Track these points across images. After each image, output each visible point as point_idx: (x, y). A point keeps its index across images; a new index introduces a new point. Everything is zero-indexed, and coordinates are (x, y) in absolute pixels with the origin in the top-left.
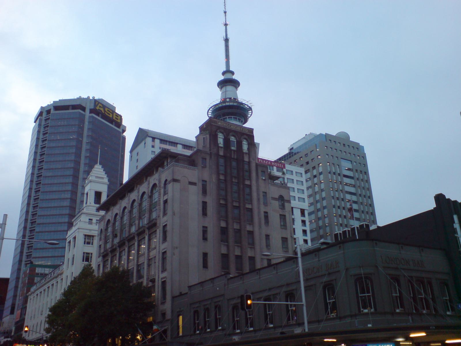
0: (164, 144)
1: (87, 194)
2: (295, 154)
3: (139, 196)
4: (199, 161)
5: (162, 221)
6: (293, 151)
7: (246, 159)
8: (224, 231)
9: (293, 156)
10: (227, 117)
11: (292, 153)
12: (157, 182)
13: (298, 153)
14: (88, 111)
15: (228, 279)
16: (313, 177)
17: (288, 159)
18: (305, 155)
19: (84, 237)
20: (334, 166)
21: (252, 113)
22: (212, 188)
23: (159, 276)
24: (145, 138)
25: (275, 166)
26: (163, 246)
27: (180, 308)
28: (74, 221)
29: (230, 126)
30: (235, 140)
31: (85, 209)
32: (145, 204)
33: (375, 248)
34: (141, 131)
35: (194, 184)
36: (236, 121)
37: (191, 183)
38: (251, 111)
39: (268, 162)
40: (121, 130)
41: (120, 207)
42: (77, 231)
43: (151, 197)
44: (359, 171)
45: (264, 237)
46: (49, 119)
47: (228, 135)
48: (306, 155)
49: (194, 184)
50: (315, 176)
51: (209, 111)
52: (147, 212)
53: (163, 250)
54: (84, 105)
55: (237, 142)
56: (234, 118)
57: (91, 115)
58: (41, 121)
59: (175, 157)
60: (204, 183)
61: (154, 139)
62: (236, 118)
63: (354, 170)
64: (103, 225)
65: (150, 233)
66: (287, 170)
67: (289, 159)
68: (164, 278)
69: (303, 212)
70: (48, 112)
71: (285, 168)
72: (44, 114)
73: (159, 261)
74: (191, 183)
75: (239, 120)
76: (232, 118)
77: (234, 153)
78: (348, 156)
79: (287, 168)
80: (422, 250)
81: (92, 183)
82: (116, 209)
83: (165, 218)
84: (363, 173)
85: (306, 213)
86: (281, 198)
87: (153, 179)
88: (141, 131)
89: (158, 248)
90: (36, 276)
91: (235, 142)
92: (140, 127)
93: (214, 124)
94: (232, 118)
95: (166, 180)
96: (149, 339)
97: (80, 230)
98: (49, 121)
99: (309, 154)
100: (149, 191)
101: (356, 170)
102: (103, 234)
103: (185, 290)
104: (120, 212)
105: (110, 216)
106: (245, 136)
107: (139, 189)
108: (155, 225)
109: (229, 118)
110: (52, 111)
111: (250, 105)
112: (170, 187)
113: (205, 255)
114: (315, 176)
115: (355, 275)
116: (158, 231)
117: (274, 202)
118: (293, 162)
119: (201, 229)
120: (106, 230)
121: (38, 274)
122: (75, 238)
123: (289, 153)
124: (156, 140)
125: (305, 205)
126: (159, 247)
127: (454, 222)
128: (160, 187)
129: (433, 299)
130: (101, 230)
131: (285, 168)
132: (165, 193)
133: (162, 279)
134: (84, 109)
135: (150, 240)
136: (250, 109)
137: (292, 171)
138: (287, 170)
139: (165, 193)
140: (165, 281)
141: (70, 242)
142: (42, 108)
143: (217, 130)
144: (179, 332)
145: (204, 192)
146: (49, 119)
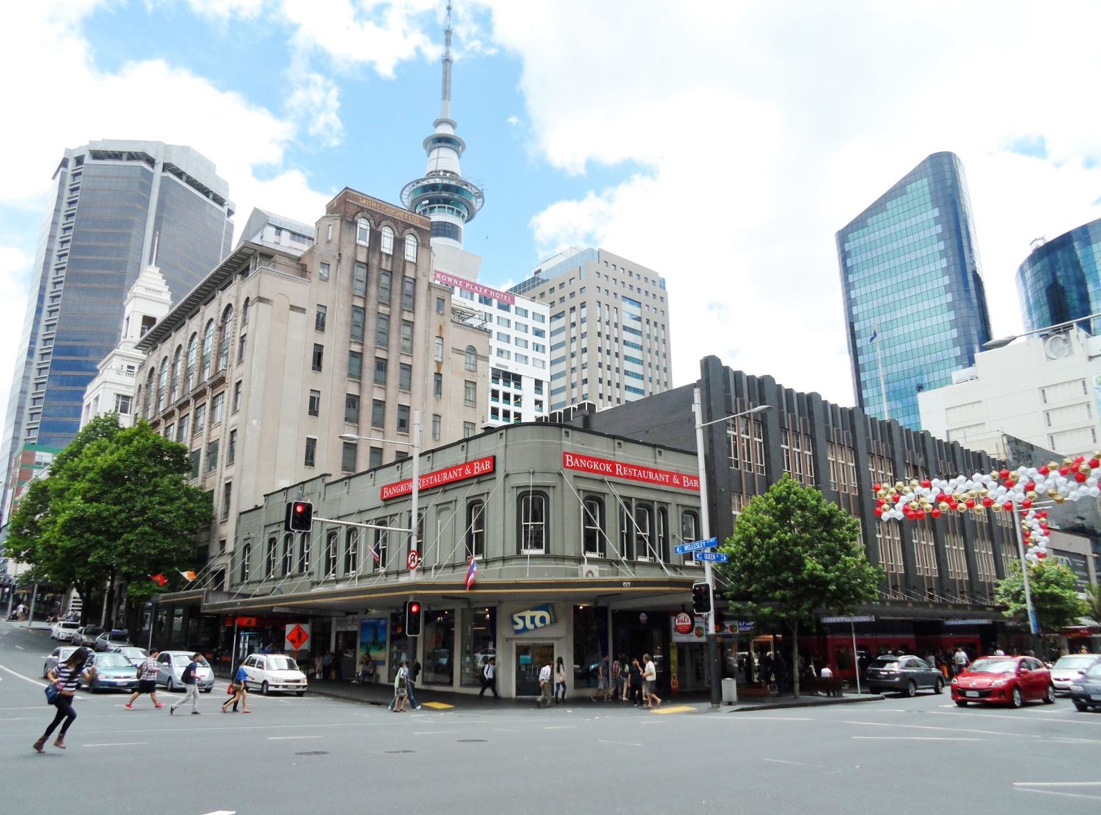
0: (298, 241)
1: (128, 319)
2: (544, 281)
3: (202, 325)
4: (316, 269)
5: (233, 376)
6: (541, 276)
7: (410, 273)
8: (353, 402)
9: (538, 284)
10: (437, 205)
11: (538, 279)
12: (233, 302)
13: (548, 280)
14: (159, 167)
15: (327, 485)
16: (569, 325)
17: (529, 289)
18: (560, 285)
19: (115, 397)
20: (600, 306)
21: (483, 202)
22: (338, 321)
23: (221, 474)
24: (264, 226)
25: (495, 298)
26: (233, 420)
27: (249, 534)
28: (101, 367)
29: (385, 209)
30: (369, 228)
31: (121, 347)
32: (211, 343)
33: (563, 442)
34: (257, 213)
35: (303, 310)
36: (453, 214)
37: (293, 308)
38: (481, 200)
39: (483, 290)
40: (225, 210)
41: (173, 345)
42: (103, 386)
43: (221, 329)
44: (652, 323)
45: (431, 418)
46: (79, 174)
47: (378, 225)
48: (562, 285)
49: (303, 310)
50: (574, 325)
51: (404, 192)
52: (212, 356)
53: (233, 426)
54: (151, 154)
55: (371, 230)
56: (448, 208)
57: (165, 174)
58: (63, 174)
59: (268, 256)
60: (322, 310)
61: (279, 229)
62: (453, 209)
63: (644, 321)
64: (142, 378)
65: (214, 395)
66: (516, 307)
67: (532, 290)
68: (229, 478)
69: (538, 384)
70: (79, 161)
71: (514, 304)
72: (72, 164)
73: (224, 447)
74: (293, 308)
75: (459, 213)
76: (445, 207)
77: (387, 260)
78: (634, 295)
79: (517, 305)
80: (660, 452)
81: (138, 299)
82: (166, 349)
83: (241, 369)
84: (659, 326)
85: (545, 387)
86: (472, 350)
87: (225, 297)
88: (257, 213)
89: (223, 423)
90: (37, 468)
91: (368, 232)
92: (260, 207)
93: (351, 201)
94: (445, 207)
95: (248, 299)
96: (1077, 630)
97: (108, 385)
98: (79, 179)
99: (567, 283)
100: (218, 317)
101: (655, 323)
102: (143, 392)
103: (261, 502)
104: (171, 355)
105: (154, 360)
106: (412, 230)
107: (204, 312)
108: (222, 381)
109: (439, 207)
110: (88, 160)
111: (480, 188)
112: (252, 310)
113: (311, 444)
114: (574, 325)
115: (518, 487)
116: (226, 394)
117: (456, 357)
118: (538, 296)
119: (308, 395)
120: (148, 386)
121: (39, 463)
122: (97, 399)
123: (534, 279)
124: (283, 232)
125: (545, 376)
126: (226, 421)
127: (693, 402)
128: (237, 310)
129: (651, 539)
130: (140, 385)
131: (514, 304)
132: (244, 322)
133: (226, 479)
134: (151, 162)
135: (213, 408)
136: (480, 195)
137: (526, 311)
138: (516, 307)
139: (244, 322)
140: (230, 483)
141: (88, 406)
142: (68, 151)
143: (358, 212)
144: (968, 618)
145: (320, 325)
146: (79, 174)
